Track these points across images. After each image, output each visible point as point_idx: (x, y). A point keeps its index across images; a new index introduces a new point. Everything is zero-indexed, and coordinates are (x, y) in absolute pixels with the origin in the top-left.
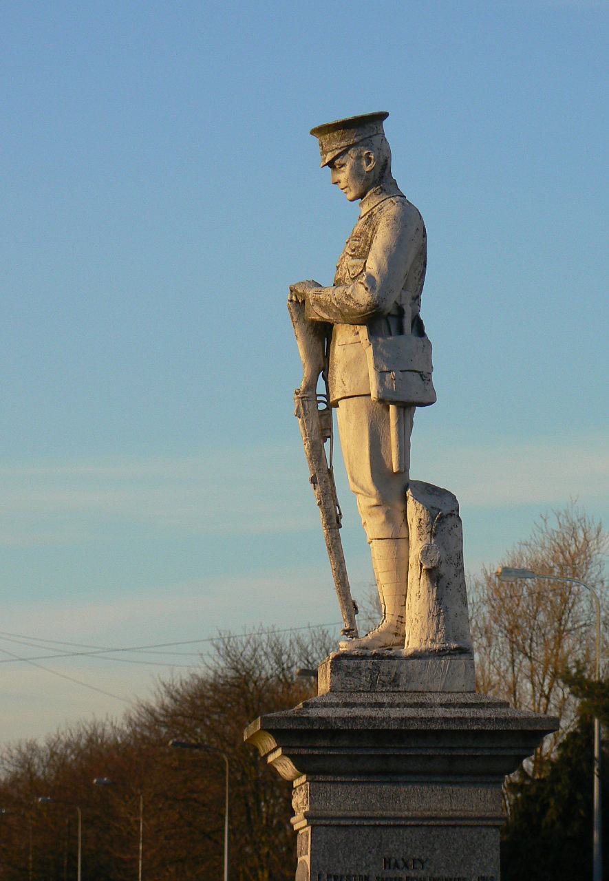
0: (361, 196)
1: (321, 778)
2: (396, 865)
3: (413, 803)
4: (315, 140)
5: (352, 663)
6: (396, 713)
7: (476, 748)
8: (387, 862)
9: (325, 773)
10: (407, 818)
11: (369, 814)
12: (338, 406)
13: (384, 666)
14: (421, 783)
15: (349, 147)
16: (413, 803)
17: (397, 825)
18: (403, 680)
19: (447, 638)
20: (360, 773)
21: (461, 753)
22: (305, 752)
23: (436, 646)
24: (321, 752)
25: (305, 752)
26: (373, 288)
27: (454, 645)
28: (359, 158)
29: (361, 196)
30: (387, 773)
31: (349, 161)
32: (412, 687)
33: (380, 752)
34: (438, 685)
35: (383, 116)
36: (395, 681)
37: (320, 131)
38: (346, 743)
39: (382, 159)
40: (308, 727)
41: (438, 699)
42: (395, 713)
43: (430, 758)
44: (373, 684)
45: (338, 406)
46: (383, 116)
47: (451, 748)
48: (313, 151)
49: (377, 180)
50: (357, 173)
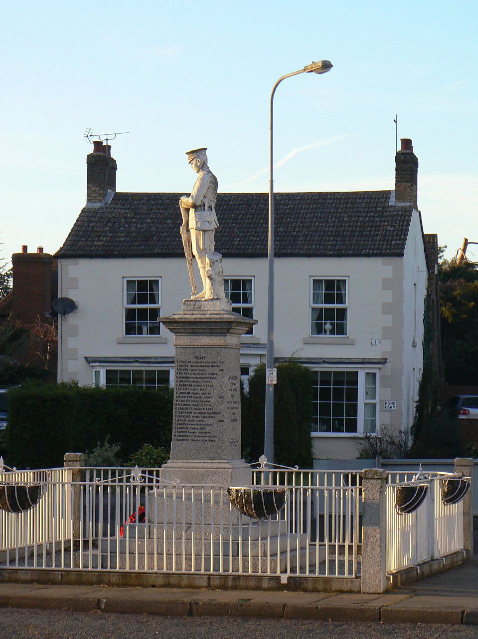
0: (198, 172)
1: (178, 334)
2: (198, 358)
3: (202, 341)
4: (187, 155)
5: (189, 303)
6: (199, 316)
7: (216, 326)
8: (196, 357)
9: (178, 333)
10: (200, 345)
11: (190, 344)
12: (434, 237)
13: (198, 303)
14: (216, 336)
15: (194, 158)
16: (202, 341)
17: (198, 347)
18: (202, 308)
19: (214, 296)
20: (188, 333)
21: (212, 327)
22: (171, 327)
23: (211, 298)
24: (176, 327)
25: (171, 327)
26: (193, 199)
27: (216, 297)
28: (196, 161)
29: (198, 172)
30: (194, 333)
31: (194, 162)
32: (205, 309)
33: (191, 327)
34: (212, 309)
35: (206, 149)
36: (200, 308)
37: (186, 153)
38: (181, 325)
39: (203, 161)
40: (170, 320)
41: (209, 312)
42: (197, 316)
43: (205, 329)
44: (194, 308)
45: (434, 237)
46: (206, 149)
47: (210, 326)
48: (187, 158)
49: (203, 166)
50: (196, 165)
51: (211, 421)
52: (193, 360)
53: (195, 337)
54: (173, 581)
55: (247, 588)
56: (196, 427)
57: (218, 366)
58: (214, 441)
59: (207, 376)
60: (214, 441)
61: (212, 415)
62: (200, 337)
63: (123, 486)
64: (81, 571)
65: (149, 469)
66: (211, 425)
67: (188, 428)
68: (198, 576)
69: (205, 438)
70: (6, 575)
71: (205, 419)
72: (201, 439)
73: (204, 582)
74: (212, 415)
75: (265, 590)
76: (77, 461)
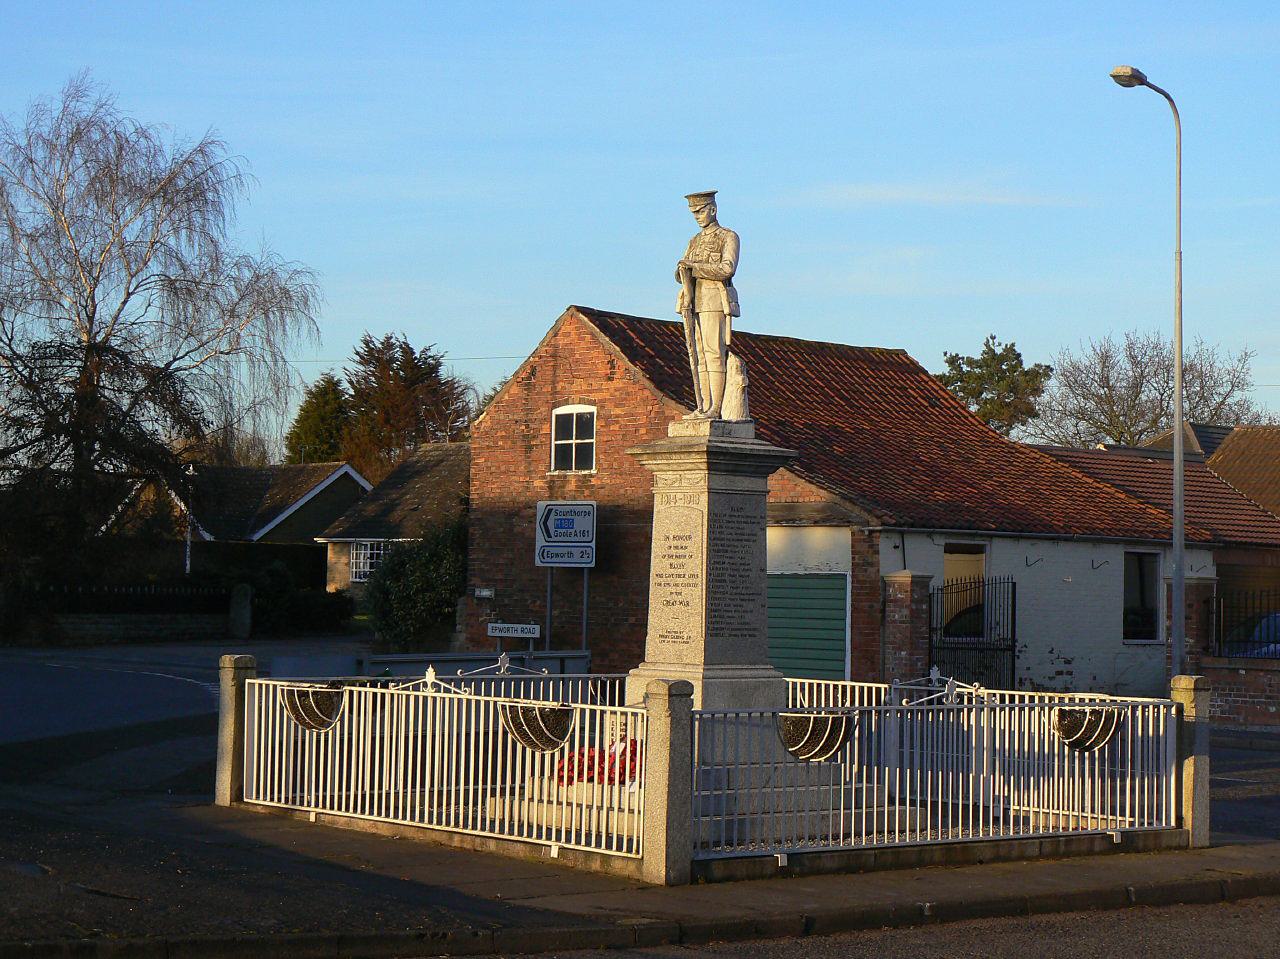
17: (735, 493)
51: (751, 606)
52: (728, 512)
53: (732, 478)
54: (1003, 852)
55: (1079, 854)
56: (733, 614)
57: (759, 523)
58: (755, 636)
59: (746, 537)
60: (755, 636)
61: (751, 597)
62: (737, 478)
63: (595, 710)
64: (1022, 839)
65: (1039, 694)
66: (751, 611)
67: (723, 617)
68: (1030, 841)
69: (745, 632)
70: (807, 862)
71: (744, 603)
72: (738, 633)
73: (938, 856)
74: (751, 597)
75: (1098, 854)
76: (252, 668)
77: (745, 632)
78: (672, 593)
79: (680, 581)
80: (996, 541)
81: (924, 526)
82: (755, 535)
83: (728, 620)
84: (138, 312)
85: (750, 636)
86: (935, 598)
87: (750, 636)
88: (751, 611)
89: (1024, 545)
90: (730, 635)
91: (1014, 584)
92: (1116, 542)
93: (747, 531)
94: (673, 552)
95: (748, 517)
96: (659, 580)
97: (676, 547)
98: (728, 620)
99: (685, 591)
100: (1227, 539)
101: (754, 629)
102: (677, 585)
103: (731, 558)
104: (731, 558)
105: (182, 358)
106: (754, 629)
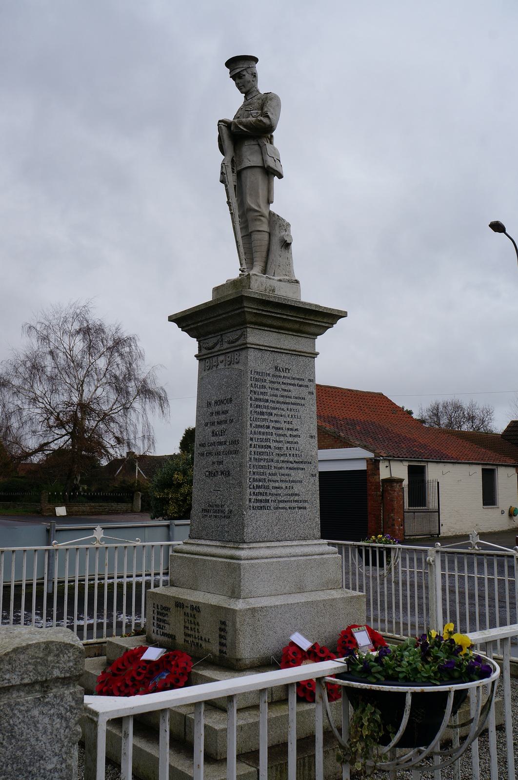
51: (300, 475)
52: (272, 371)
57: (307, 386)
58: (305, 508)
60: (305, 508)
71: (292, 472)
74: (301, 466)
77: (294, 505)
78: (214, 463)
79: (221, 448)
80: (429, 463)
81: (399, 457)
82: (304, 399)
83: (274, 491)
84: (105, 397)
85: (300, 508)
86: (405, 490)
87: (300, 508)
88: (301, 482)
89: (441, 466)
90: (277, 508)
91: (438, 483)
92: (479, 464)
93: (293, 394)
94: (215, 418)
95: (294, 379)
96: (202, 450)
97: (218, 413)
98: (274, 491)
99: (226, 460)
100: (218, 544)
101: (305, 501)
102: (218, 454)
103: (276, 422)
104: (276, 422)
105: (114, 410)
106: (305, 501)
